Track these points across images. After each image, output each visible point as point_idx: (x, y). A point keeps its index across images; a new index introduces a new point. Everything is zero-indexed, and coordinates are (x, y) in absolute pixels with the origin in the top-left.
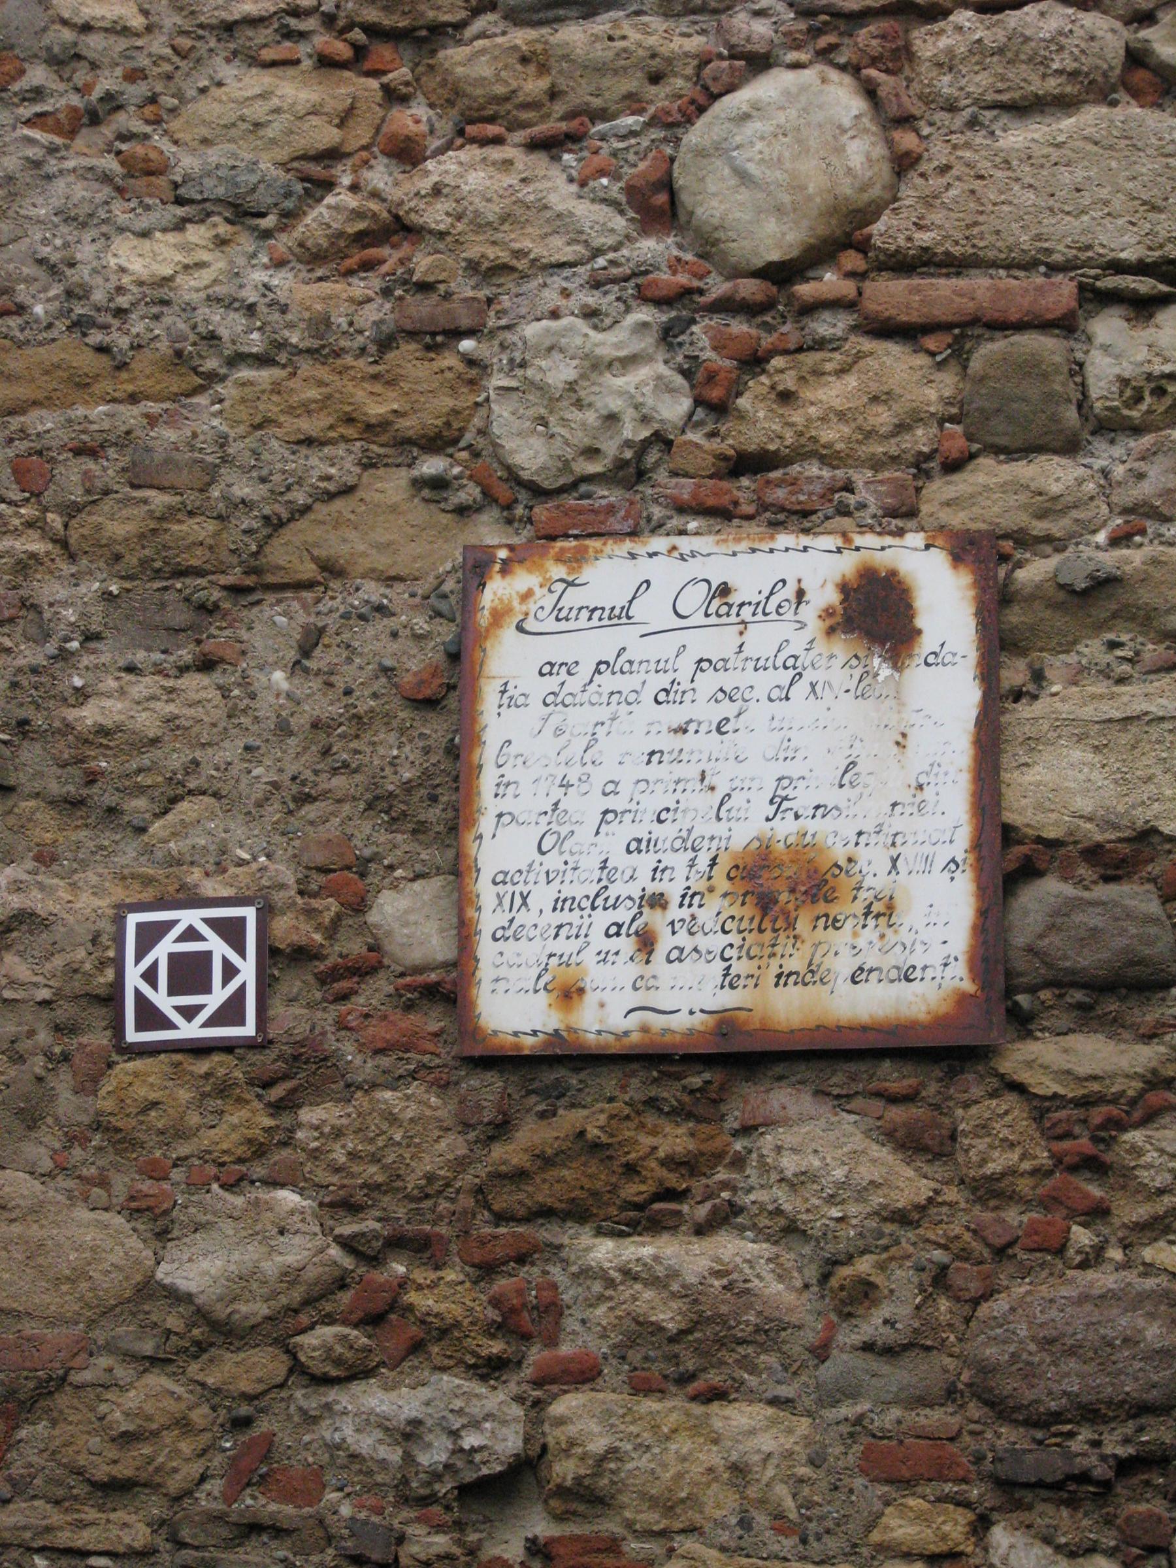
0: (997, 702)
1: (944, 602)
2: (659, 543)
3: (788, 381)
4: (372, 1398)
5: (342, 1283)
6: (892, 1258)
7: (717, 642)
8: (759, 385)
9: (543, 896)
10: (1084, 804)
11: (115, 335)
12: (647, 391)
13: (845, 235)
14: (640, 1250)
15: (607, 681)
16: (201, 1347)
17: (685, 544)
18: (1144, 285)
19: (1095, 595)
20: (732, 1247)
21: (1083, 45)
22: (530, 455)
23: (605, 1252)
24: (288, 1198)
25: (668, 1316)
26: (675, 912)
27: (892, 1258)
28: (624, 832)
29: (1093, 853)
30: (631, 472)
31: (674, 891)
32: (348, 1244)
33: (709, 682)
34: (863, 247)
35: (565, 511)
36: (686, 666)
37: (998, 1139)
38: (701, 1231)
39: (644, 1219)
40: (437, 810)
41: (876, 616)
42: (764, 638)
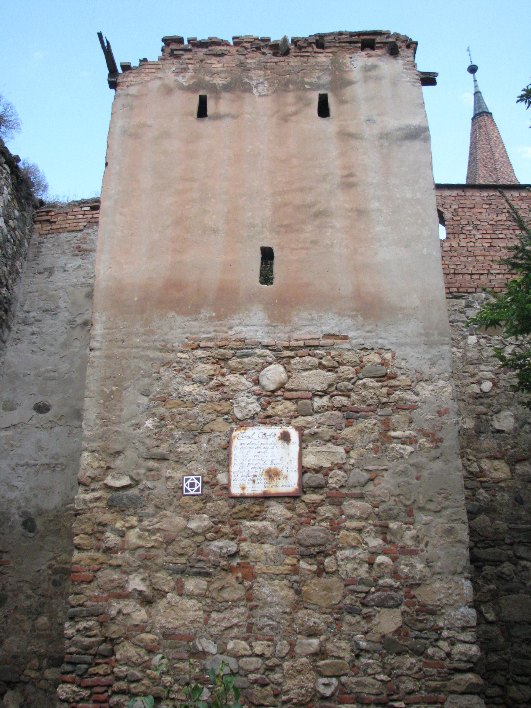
0: (301, 449)
1: (294, 435)
2: (256, 427)
3: (274, 406)
4: (216, 543)
7: (264, 441)
9: (240, 475)
12: (255, 407)
13: (281, 386)
14: (253, 523)
15: (249, 446)
20: (265, 523)
22: (239, 415)
23: (248, 523)
25: (256, 532)
29: (314, 470)
30: (253, 418)
32: (213, 522)
34: (284, 388)
35: (243, 423)
37: (301, 508)
38: (261, 521)
39: (253, 519)
41: (285, 437)
42: (270, 440)
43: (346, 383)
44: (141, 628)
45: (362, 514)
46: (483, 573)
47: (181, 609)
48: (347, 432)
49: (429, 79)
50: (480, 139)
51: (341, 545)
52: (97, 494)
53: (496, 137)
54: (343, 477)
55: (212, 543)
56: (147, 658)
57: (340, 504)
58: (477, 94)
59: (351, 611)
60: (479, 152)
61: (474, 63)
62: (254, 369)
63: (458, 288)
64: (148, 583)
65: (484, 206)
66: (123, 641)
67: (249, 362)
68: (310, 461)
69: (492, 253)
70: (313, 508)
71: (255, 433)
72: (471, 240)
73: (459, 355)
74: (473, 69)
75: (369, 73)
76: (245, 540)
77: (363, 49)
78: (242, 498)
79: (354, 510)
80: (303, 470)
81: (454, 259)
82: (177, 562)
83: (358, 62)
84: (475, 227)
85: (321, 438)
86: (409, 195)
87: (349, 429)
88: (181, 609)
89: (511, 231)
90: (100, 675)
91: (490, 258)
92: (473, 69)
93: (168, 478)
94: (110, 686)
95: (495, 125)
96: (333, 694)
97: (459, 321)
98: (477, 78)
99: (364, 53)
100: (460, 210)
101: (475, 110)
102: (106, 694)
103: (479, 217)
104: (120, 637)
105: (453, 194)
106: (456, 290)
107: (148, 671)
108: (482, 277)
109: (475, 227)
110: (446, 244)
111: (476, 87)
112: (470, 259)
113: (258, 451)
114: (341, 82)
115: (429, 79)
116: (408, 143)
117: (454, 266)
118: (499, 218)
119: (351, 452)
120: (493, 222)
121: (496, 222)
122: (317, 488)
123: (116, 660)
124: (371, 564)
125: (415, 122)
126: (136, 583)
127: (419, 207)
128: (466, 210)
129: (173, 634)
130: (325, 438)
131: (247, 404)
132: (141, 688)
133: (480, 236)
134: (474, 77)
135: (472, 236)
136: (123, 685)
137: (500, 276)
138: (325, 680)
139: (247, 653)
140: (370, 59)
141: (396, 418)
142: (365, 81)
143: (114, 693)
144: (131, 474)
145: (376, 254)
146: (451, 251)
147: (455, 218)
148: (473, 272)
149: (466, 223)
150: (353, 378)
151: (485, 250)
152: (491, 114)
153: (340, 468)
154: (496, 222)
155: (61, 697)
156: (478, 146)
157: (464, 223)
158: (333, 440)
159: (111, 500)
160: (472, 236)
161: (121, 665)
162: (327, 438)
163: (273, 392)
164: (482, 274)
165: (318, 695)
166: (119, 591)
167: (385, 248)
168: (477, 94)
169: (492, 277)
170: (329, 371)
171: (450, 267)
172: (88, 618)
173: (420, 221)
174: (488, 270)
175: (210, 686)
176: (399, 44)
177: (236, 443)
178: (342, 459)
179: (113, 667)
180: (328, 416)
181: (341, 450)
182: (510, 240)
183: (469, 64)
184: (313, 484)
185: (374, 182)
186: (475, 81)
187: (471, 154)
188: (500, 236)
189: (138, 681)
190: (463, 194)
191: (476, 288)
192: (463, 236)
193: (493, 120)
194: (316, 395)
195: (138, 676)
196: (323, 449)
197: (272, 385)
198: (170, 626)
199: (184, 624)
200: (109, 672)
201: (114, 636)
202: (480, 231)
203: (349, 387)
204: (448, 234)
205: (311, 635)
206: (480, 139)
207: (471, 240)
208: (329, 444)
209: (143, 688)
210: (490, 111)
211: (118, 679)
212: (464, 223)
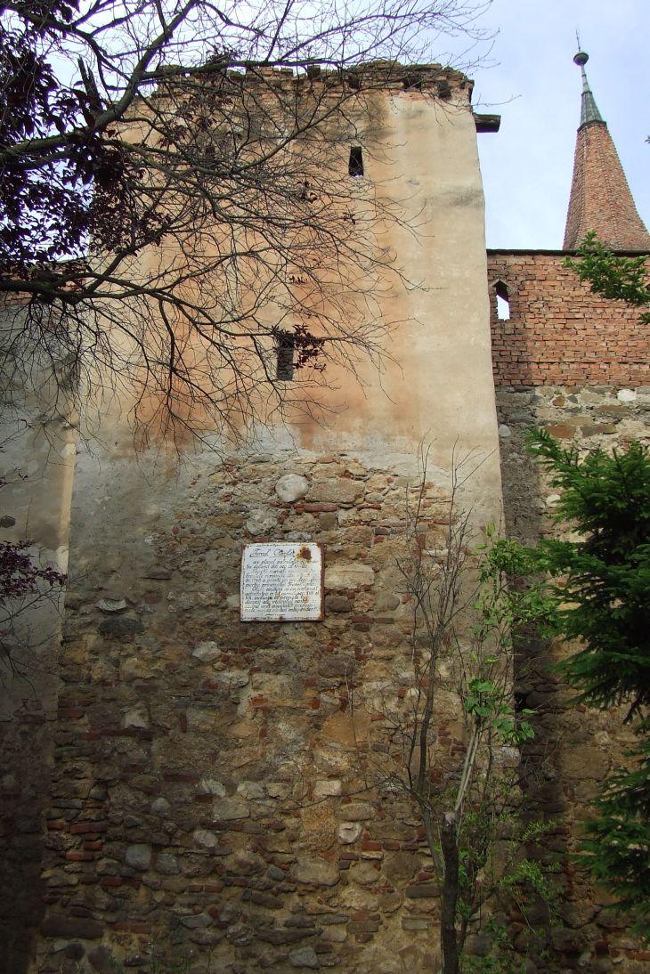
0: (324, 566)
1: (316, 553)
2: (272, 544)
3: (292, 519)
4: (226, 674)
5: (220, 656)
6: (209, 174)
7: (282, 559)
8: (288, 520)
9: (253, 597)
10: (337, 584)
11: (324, 906)
12: (270, 522)
13: (301, 498)
14: (267, 651)
15: (264, 565)
16: (199, 665)
17: (276, 544)
18: (347, 506)
19: (338, 553)
20: (281, 651)
21: (346, 536)
22: (253, 530)
23: (261, 651)
24: (213, 643)
25: (272, 661)
26: (273, 600)
27: (209, 174)
28: (266, 588)
29: (338, 592)
30: (268, 533)
31: (273, 596)
32: (222, 650)
33: (279, 565)
34: (304, 499)
35: (253, 538)
36: (276, 562)
37: (326, 636)
38: (276, 648)
39: (267, 647)
40: (236, 585)
41: (306, 554)
42: (288, 559)
43: (375, 494)
44: (136, 768)
45: (391, 641)
46: (543, 722)
47: (185, 747)
48: (375, 550)
49: (488, 124)
50: (589, 159)
51: (367, 676)
52: (88, 619)
53: (611, 156)
54: (372, 600)
55: (221, 674)
56: (145, 802)
57: (366, 629)
58: (587, 95)
59: (377, 749)
60: (586, 178)
61: (583, 50)
62: (270, 476)
63: (521, 380)
64: (147, 719)
65: (558, 278)
66: (118, 784)
67: (264, 470)
68: (335, 579)
69: (566, 337)
70: (336, 634)
71: (270, 550)
72: (541, 320)
73: (520, 461)
74: (581, 59)
75: (413, 122)
76: (258, 670)
77: (406, 87)
78: (255, 623)
79: (383, 637)
80: (326, 592)
81: (518, 344)
82: (180, 694)
83: (398, 105)
84: (546, 304)
85: (347, 556)
86: (455, 274)
87: (377, 546)
88: (185, 747)
89: (591, 310)
90: (93, 821)
91: (563, 343)
92: (581, 59)
93: (170, 601)
94: (104, 832)
95: (609, 139)
96: (356, 840)
97: (522, 420)
98: (587, 72)
99: (408, 94)
100: (528, 282)
101: (582, 118)
102: (99, 841)
103: (552, 291)
104: (115, 779)
105: (520, 263)
106: (519, 382)
107: (147, 816)
108: (552, 367)
109: (546, 304)
110: (509, 326)
111: (586, 84)
112: (538, 344)
113: (275, 569)
114: (377, 132)
115: (488, 124)
116: (458, 210)
117: (519, 354)
118: (577, 293)
119: (381, 572)
120: (568, 299)
121: (572, 298)
122: (340, 612)
123: (111, 805)
124: (401, 697)
125: (467, 183)
126: (134, 719)
127: (468, 289)
128: (535, 282)
129: (177, 775)
130: (351, 556)
131: (262, 518)
132: (139, 835)
133: (551, 316)
134: (583, 70)
135: (541, 316)
136: (119, 830)
137: (575, 366)
138: (349, 825)
139: (260, 795)
140: (415, 102)
141: (430, 536)
142: (408, 132)
143: (109, 840)
144: (129, 596)
145: (414, 344)
146: (514, 334)
147: (521, 293)
148: (541, 361)
149: (535, 299)
150: (383, 489)
151: (557, 332)
152: (605, 123)
153: (367, 591)
154: (572, 298)
155: (47, 845)
156: (585, 170)
157: (532, 298)
158: (360, 557)
159: (106, 625)
160: (541, 316)
161: (116, 810)
162: (353, 556)
163: (291, 503)
164: (552, 363)
165: (340, 841)
166: (113, 728)
167: (425, 338)
168: (587, 95)
169: (564, 367)
170: (357, 479)
171: (513, 354)
172: (77, 759)
173: (467, 306)
174: (560, 358)
175: (218, 832)
176: (450, 83)
177: (247, 561)
178: (371, 580)
179: (107, 812)
180: (355, 531)
181: (369, 569)
182: (589, 321)
183: (577, 52)
184: (337, 608)
185: (415, 257)
186: (584, 75)
187: (575, 180)
188: (577, 316)
189: (136, 826)
190: (532, 262)
191: (544, 381)
192: (531, 316)
193: (607, 132)
194: (342, 508)
195: (136, 822)
196: (349, 568)
197: (290, 495)
198: (173, 766)
199: (188, 763)
200: (103, 817)
201: (108, 778)
202: (552, 310)
203: (379, 499)
204: (511, 312)
205: (332, 777)
206: (589, 159)
207: (541, 320)
208: (355, 563)
209: (142, 835)
210: (604, 120)
211: (114, 824)
212: (532, 298)
